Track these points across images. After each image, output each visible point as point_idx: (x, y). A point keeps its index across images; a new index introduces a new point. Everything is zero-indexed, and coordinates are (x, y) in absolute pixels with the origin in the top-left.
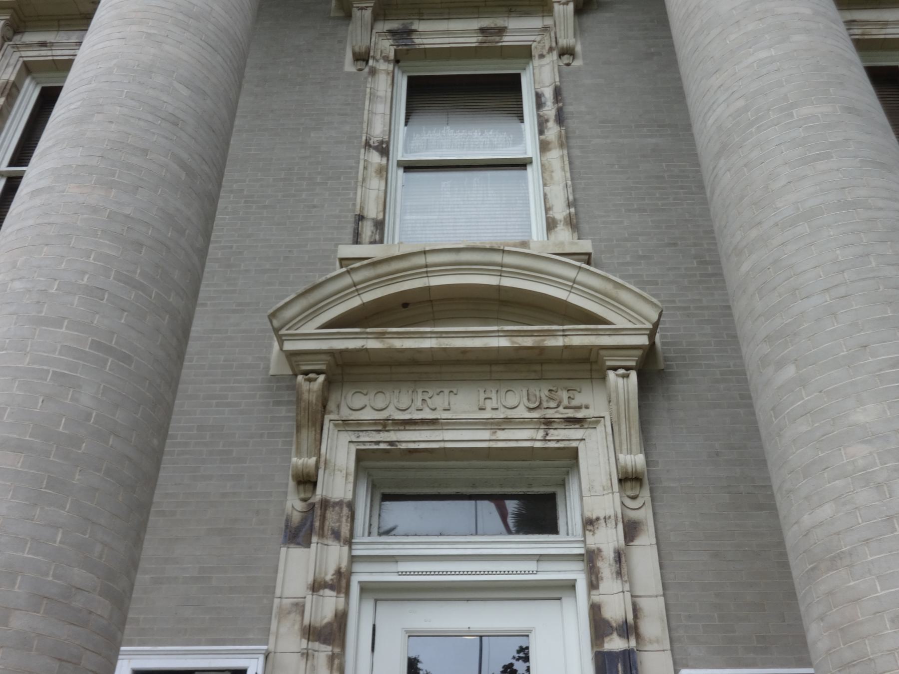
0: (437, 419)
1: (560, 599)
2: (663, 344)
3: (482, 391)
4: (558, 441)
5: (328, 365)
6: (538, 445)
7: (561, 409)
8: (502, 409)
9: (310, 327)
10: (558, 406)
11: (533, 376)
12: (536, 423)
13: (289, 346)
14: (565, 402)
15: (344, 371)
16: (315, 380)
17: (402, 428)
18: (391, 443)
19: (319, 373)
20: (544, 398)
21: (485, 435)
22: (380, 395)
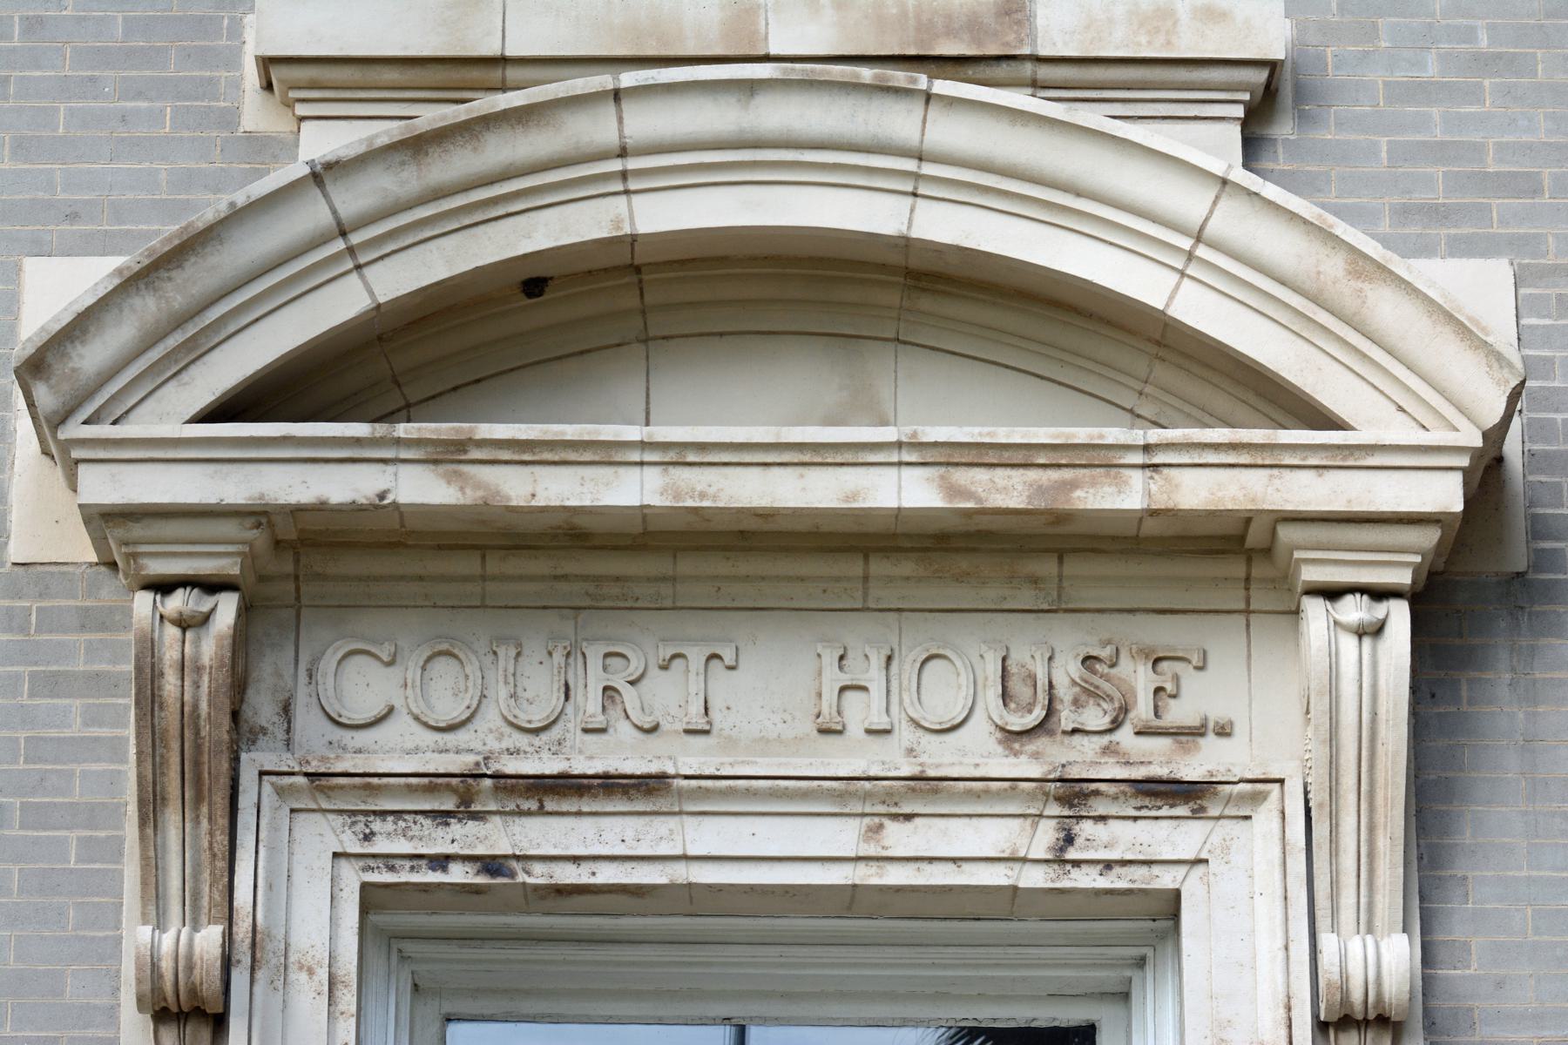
0: (662, 776)
1: (1248, 818)
2: (1530, 456)
3: (830, 657)
4: (1108, 865)
5: (250, 558)
6: (1035, 878)
7: (1125, 736)
8: (905, 734)
9: (170, 413)
10: (1116, 725)
11: (1026, 598)
12: (1031, 796)
13: (107, 486)
14: (1143, 709)
15: (300, 574)
16: (206, 619)
17: (533, 805)
18: (491, 865)
19: (211, 586)
20: (1064, 692)
21: (842, 836)
22: (442, 666)
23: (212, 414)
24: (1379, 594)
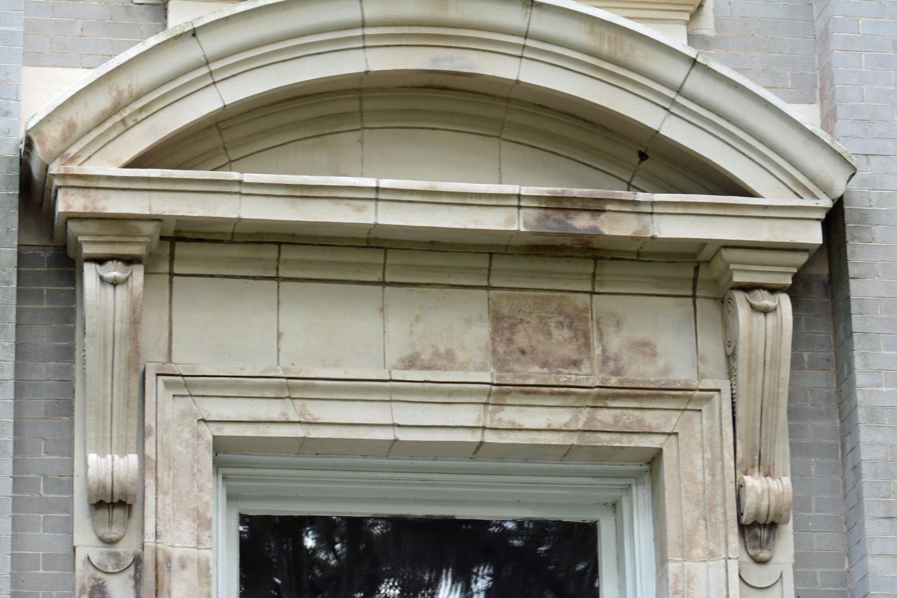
21: (468, 415)
23: (134, 164)
24: (773, 290)
